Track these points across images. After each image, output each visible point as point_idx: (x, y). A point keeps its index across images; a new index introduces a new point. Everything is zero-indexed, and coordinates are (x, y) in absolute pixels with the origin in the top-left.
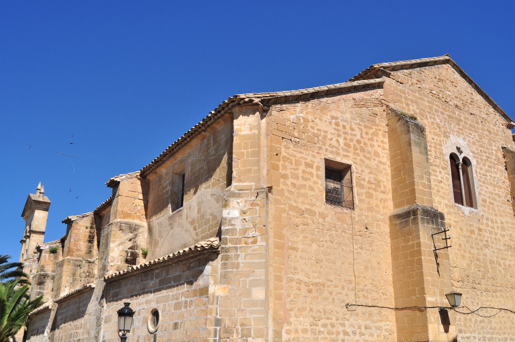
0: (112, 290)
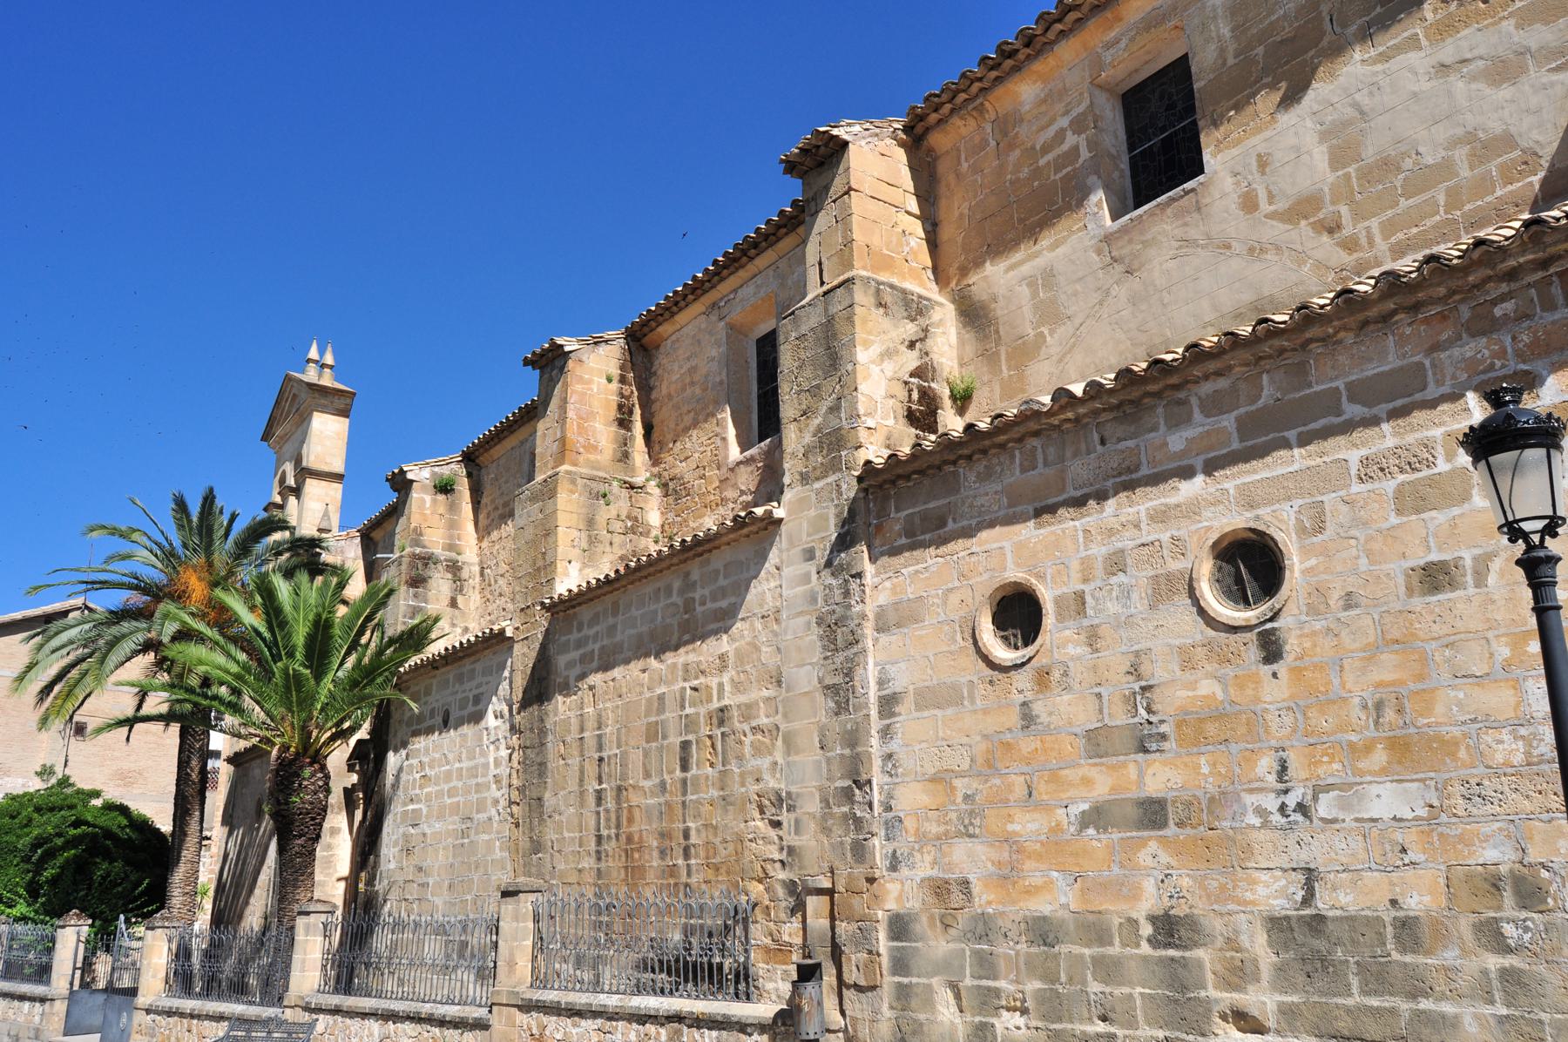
0: (898, 510)
